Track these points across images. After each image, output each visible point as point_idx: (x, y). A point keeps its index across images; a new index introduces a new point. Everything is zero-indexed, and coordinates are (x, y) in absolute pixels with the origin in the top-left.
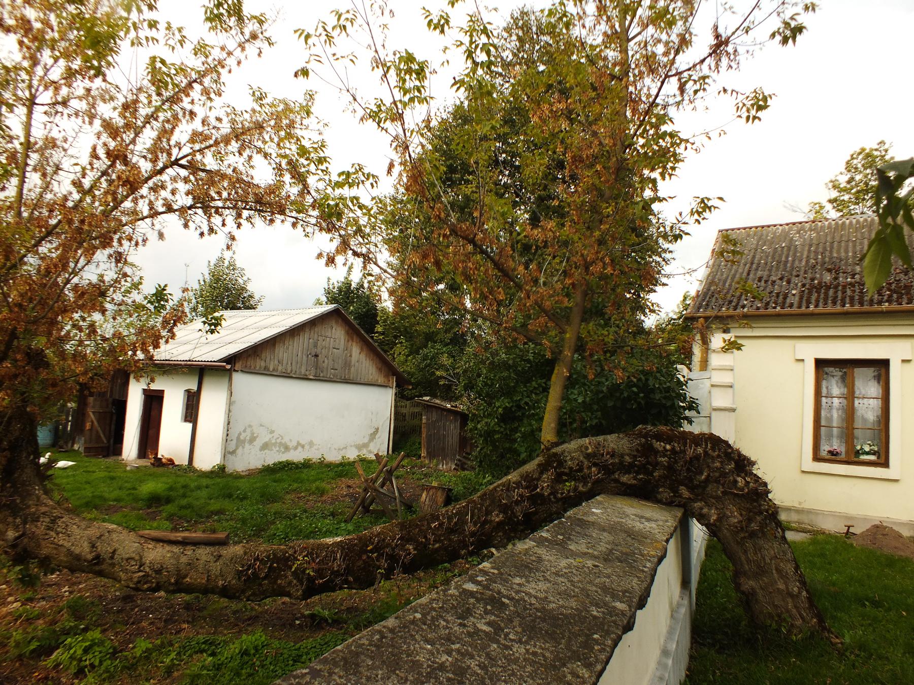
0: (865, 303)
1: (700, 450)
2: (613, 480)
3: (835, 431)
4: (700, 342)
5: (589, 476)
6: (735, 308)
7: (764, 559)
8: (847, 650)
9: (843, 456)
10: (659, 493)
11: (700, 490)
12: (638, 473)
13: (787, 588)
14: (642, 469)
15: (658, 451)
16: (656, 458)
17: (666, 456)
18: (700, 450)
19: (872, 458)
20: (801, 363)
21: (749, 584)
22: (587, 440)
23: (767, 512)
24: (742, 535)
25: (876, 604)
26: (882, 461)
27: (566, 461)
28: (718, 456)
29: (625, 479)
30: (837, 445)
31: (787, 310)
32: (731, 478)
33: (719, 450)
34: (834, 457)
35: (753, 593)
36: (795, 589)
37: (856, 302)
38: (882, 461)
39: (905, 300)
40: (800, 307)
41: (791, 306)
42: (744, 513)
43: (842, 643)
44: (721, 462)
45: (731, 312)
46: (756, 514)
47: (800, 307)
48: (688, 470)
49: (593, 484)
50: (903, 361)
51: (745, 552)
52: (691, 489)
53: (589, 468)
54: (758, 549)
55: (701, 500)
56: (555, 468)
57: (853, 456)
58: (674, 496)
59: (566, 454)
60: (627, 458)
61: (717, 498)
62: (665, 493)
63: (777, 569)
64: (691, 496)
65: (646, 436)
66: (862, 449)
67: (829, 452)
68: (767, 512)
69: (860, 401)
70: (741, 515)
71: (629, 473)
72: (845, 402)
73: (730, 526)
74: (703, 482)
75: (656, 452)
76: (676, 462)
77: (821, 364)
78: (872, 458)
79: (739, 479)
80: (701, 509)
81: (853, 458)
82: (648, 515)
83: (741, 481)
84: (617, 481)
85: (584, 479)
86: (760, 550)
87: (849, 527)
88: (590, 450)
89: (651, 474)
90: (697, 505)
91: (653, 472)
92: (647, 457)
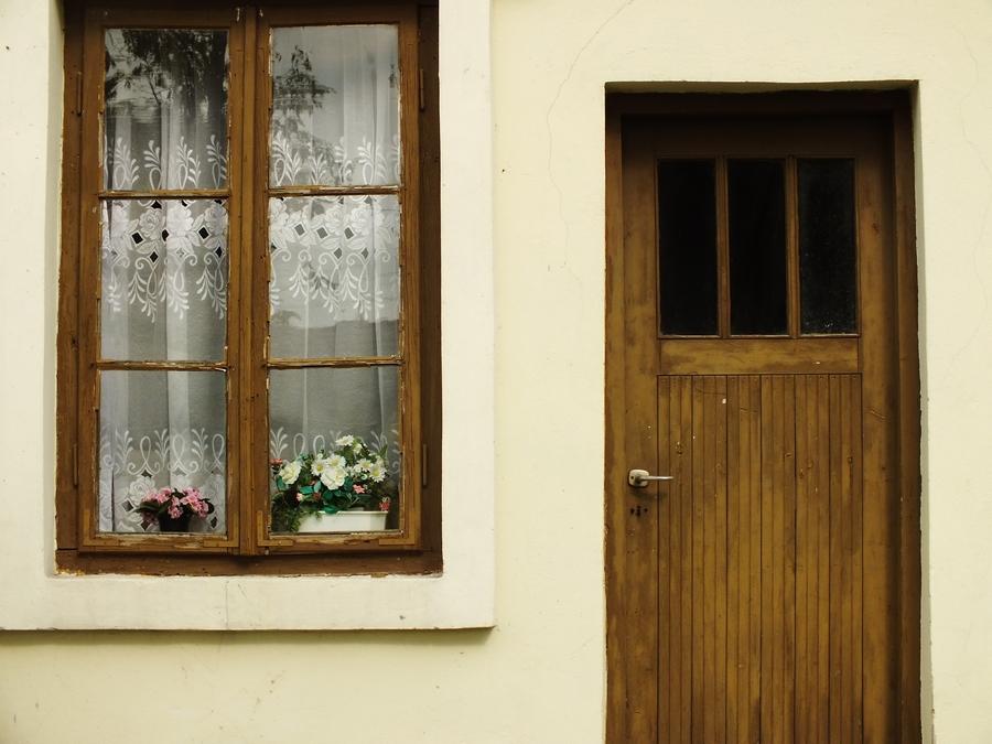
3: (180, 386)
9: (215, 536)
19: (362, 523)
30: (188, 471)
34: (173, 540)
57: (263, 522)
66: (307, 478)
67: (151, 510)
72: (215, 216)
78: (362, 523)
81: (260, 530)
82: (804, 676)
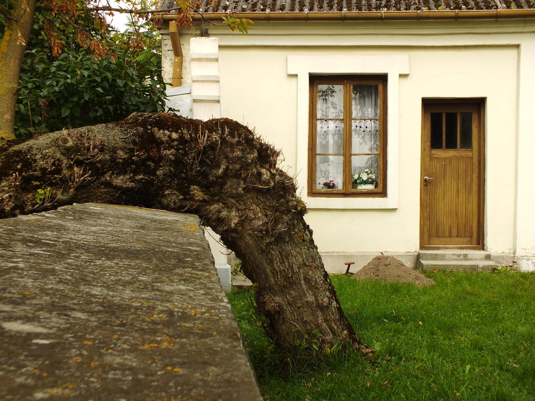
0: (364, 8)
1: (215, 137)
2: (103, 183)
4: (172, 53)
5: (71, 178)
6: (216, 9)
7: (292, 267)
8: (378, 357)
10: (164, 196)
11: (217, 188)
12: (136, 172)
13: (317, 300)
14: (141, 166)
15: (162, 142)
16: (159, 151)
17: (172, 147)
18: (215, 137)
20: (294, 80)
21: (275, 301)
22: (65, 132)
23: (296, 209)
24: (268, 240)
25: (396, 319)
26: (380, 189)
27: (35, 161)
28: (239, 143)
29: (119, 181)
31: (278, 13)
32: (255, 170)
33: (239, 136)
35: (280, 311)
36: (326, 300)
37: (354, 6)
38: (380, 189)
39: (403, 7)
40: (292, 9)
41: (282, 8)
42: (269, 213)
43: (372, 352)
44: (243, 151)
45: (210, 14)
46: (282, 213)
47: (292, 9)
48: (202, 163)
49: (77, 189)
50: (401, 76)
51: (271, 261)
52: (206, 187)
53: (70, 167)
54: (285, 256)
55: (218, 201)
56: (20, 171)
57: (350, 186)
58: (185, 199)
59: (35, 152)
60: (121, 153)
61: (238, 197)
62: (172, 196)
63: (305, 279)
64: (206, 197)
65: (144, 124)
66: (359, 178)
68: (296, 209)
69: (357, 123)
70: (266, 215)
71: (125, 173)
72: (342, 125)
73: (253, 230)
74: (220, 177)
75: (159, 143)
76: (186, 154)
77: (315, 79)
79: (264, 171)
80: (219, 212)
81: (352, 188)
83: (266, 174)
84: (108, 184)
85: (64, 183)
86: (287, 258)
87: (349, 265)
88: (70, 143)
89: (153, 172)
90: (215, 207)
91: (155, 170)
92: (147, 151)
